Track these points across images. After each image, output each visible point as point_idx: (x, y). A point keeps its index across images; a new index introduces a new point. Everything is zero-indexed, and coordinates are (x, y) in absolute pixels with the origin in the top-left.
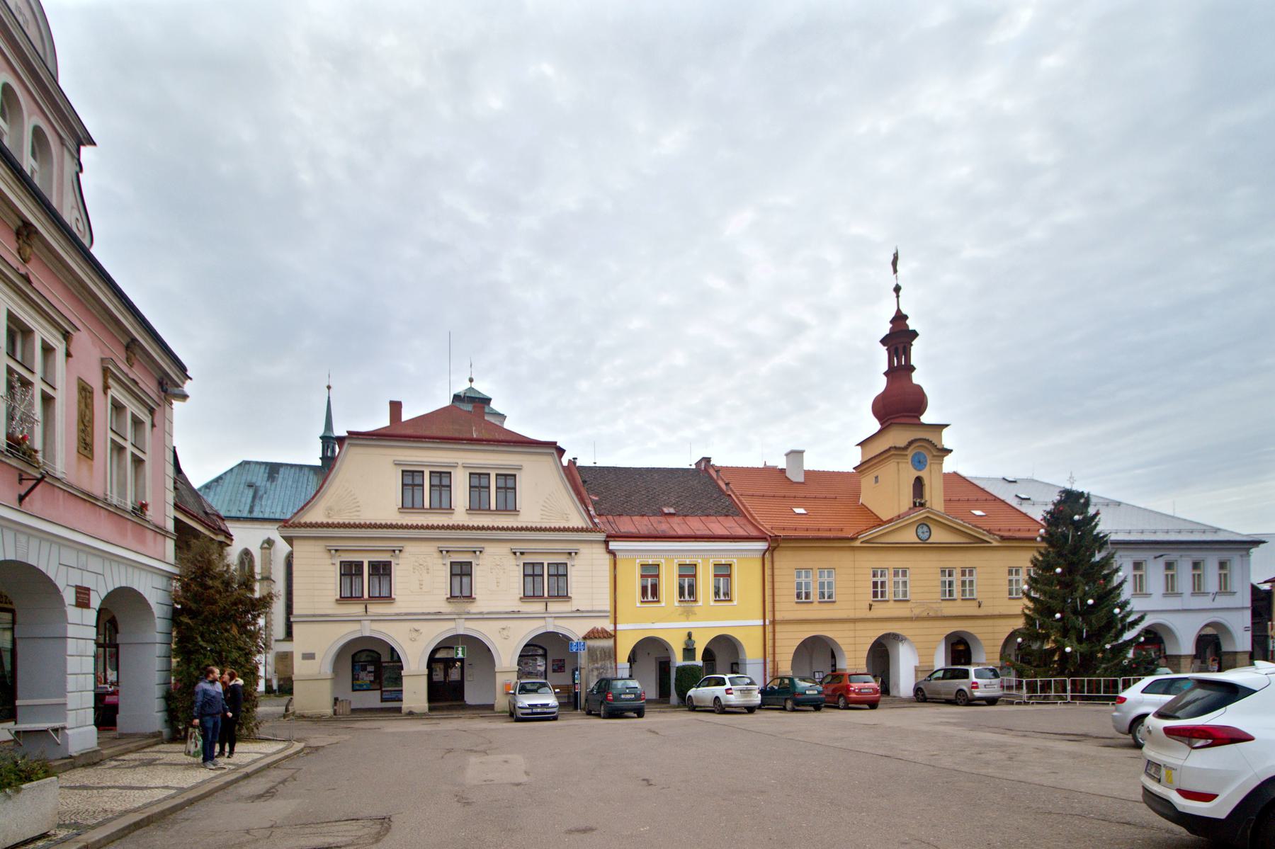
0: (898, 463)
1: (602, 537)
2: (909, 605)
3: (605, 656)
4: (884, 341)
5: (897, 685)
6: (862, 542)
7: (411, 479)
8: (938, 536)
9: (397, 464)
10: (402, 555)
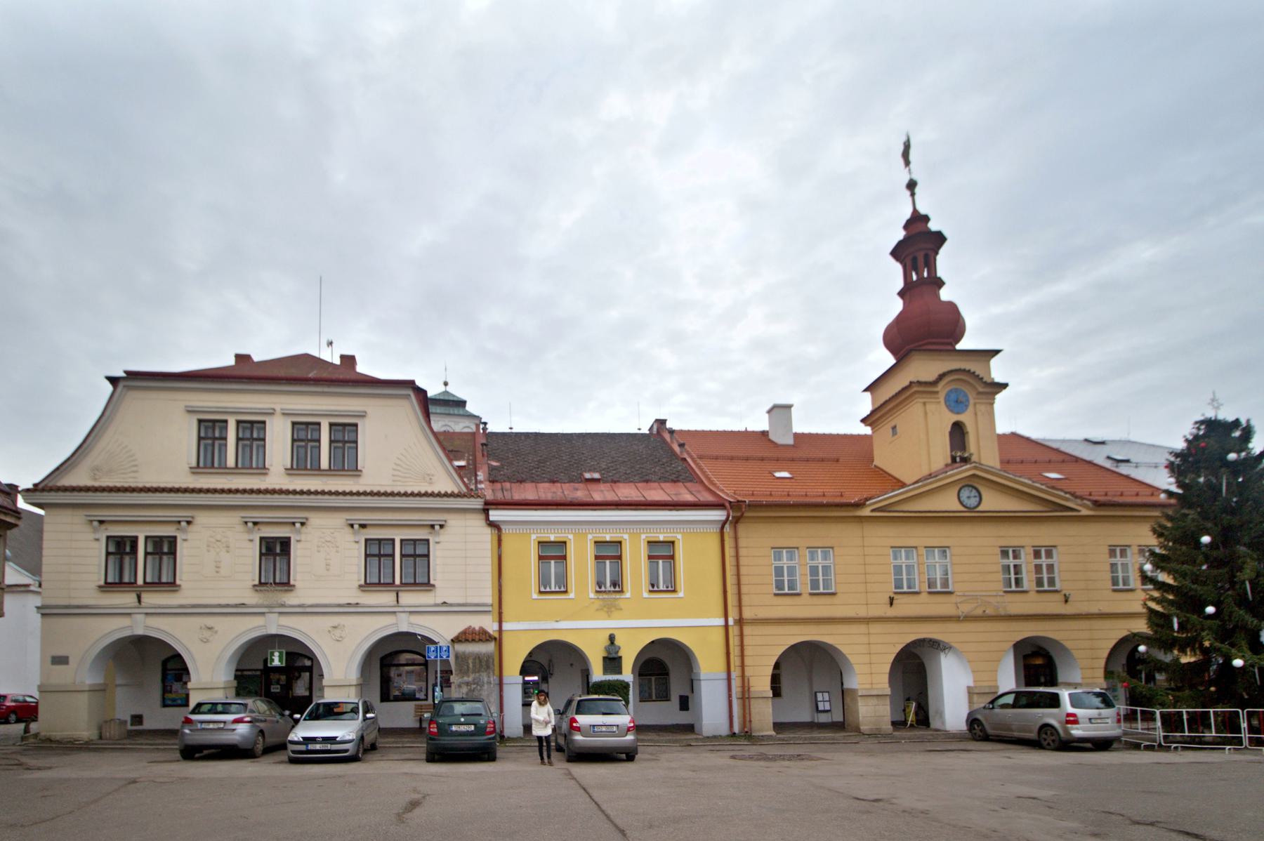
0: (924, 404)
1: (477, 504)
2: (952, 599)
3: (481, 665)
4: (897, 253)
5: (941, 714)
6: (873, 511)
7: (210, 431)
8: (992, 502)
9: (190, 411)
10: (191, 528)
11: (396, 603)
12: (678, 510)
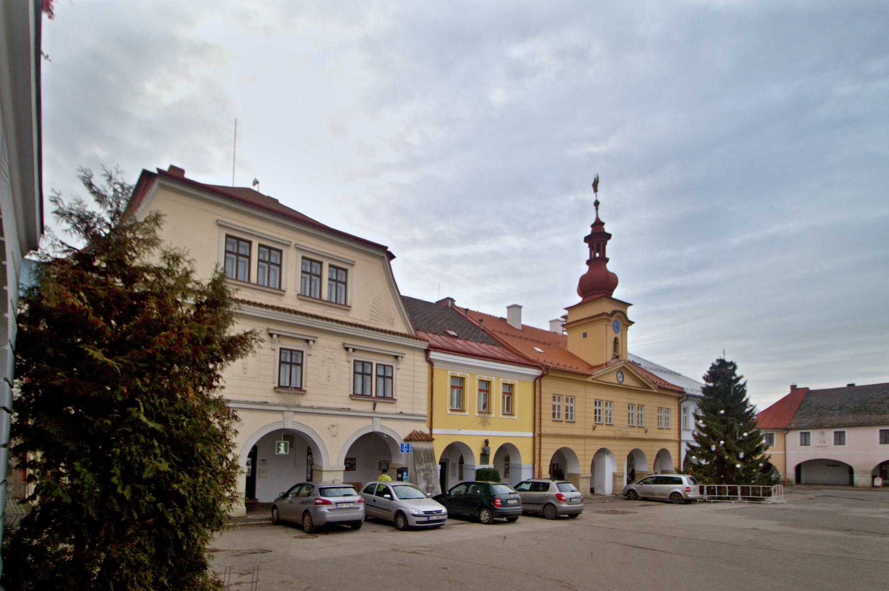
0: (606, 325)
4: (587, 239)
6: (593, 379)
9: (220, 225)
11: (372, 410)
12: (520, 366)
